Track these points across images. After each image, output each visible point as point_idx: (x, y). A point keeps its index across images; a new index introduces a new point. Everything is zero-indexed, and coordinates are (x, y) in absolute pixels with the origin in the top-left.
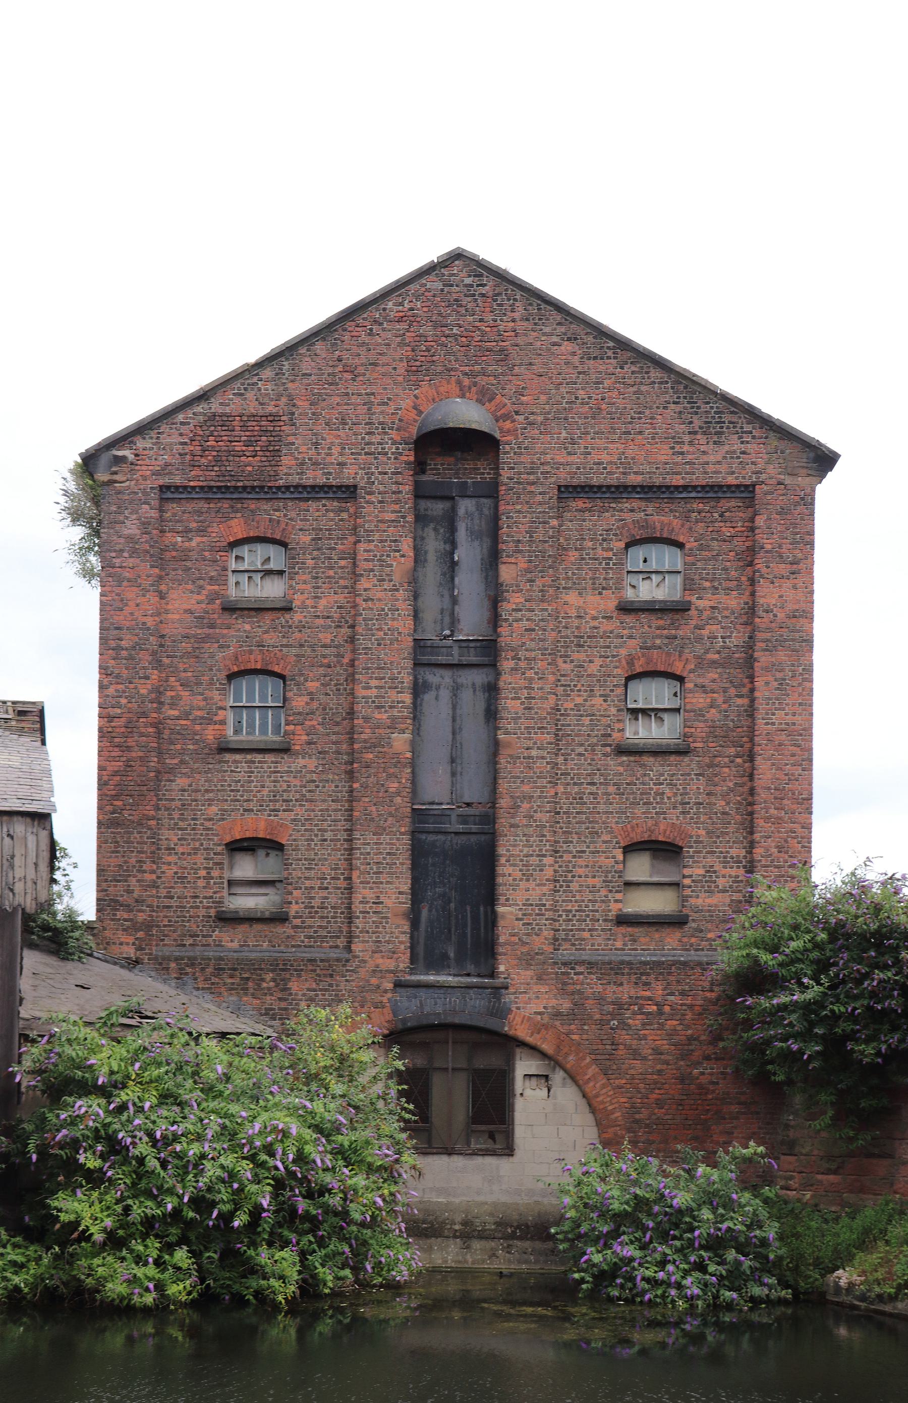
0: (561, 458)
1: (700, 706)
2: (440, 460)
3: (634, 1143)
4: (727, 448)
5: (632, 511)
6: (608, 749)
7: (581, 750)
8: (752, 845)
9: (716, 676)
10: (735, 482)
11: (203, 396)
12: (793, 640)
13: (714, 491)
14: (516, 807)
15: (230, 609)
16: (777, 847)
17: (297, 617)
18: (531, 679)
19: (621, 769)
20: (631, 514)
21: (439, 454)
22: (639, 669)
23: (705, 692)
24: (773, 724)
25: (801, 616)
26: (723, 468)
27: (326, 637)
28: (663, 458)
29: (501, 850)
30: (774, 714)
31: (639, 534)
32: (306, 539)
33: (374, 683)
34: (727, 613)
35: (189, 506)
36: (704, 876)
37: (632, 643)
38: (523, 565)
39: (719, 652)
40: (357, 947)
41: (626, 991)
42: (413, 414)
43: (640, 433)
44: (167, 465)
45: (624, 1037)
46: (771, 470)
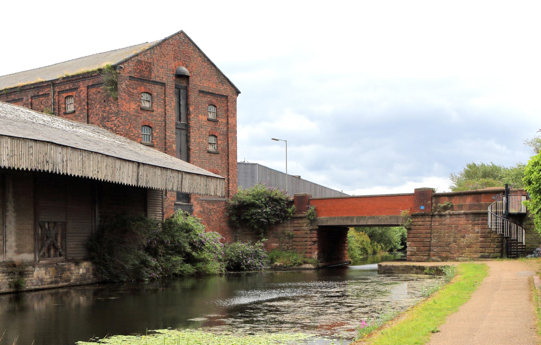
0: (199, 84)
3: (469, 172)
8: (228, 175)
11: (137, 55)
13: (222, 96)
15: (142, 109)
17: (154, 113)
20: (209, 98)
27: (160, 119)
32: (155, 94)
35: (134, 82)
40: (168, 195)
41: (211, 207)
42: (174, 68)
44: (130, 71)
45: (211, 217)
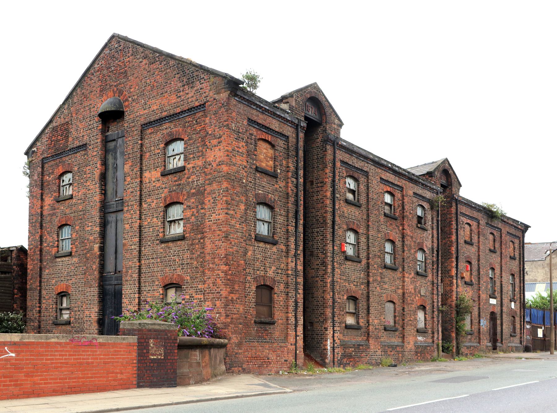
1: (188, 216)
2: (113, 124)
4: (195, 89)
5: (166, 129)
6: (158, 242)
7: (149, 243)
9: (194, 200)
10: (198, 104)
12: (219, 177)
14: (127, 272)
16: (212, 283)
18: (132, 214)
19: (162, 250)
21: (113, 122)
22: (168, 203)
23: (190, 209)
24: (211, 221)
25: (222, 164)
26: (194, 99)
28: (173, 101)
29: (123, 292)
30: (211, 216)
31: (169, 139)
33: (90, 224)
34: (198, 169)
36: (189, 299)
37: (166, 190)
38: (130, 164)
39: (195, 189)
43: (166, 92)
46: (211, 94)
